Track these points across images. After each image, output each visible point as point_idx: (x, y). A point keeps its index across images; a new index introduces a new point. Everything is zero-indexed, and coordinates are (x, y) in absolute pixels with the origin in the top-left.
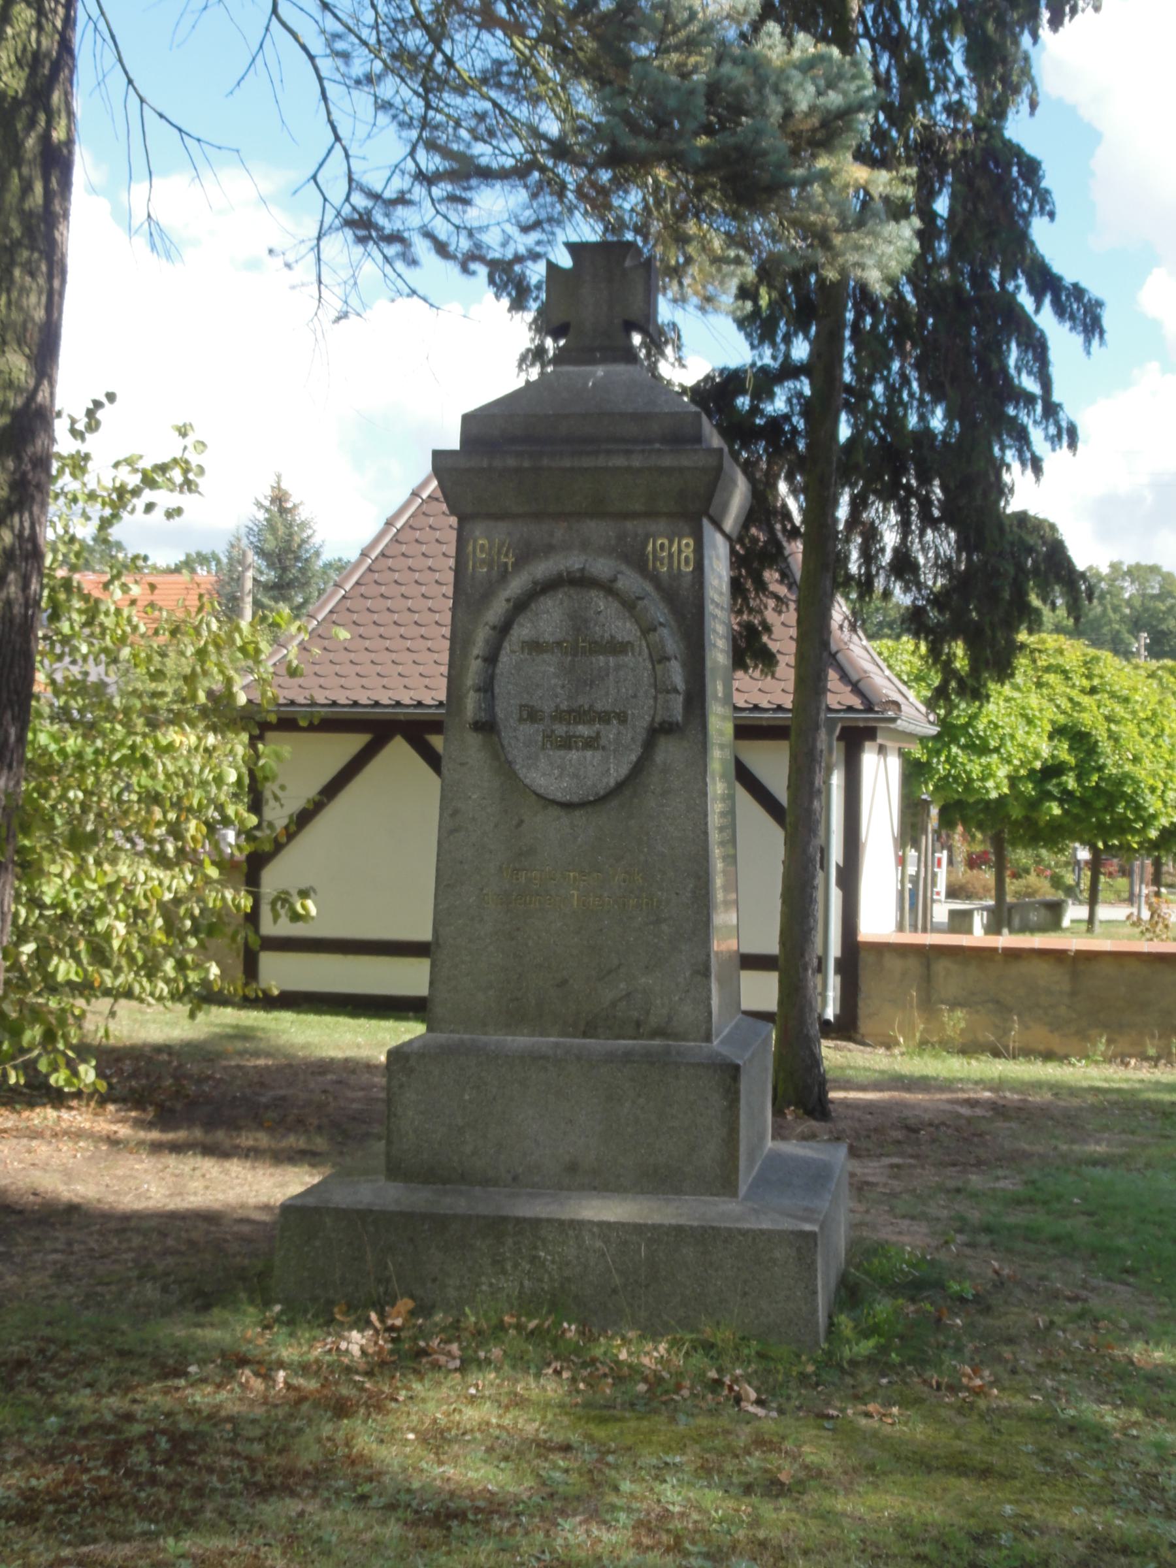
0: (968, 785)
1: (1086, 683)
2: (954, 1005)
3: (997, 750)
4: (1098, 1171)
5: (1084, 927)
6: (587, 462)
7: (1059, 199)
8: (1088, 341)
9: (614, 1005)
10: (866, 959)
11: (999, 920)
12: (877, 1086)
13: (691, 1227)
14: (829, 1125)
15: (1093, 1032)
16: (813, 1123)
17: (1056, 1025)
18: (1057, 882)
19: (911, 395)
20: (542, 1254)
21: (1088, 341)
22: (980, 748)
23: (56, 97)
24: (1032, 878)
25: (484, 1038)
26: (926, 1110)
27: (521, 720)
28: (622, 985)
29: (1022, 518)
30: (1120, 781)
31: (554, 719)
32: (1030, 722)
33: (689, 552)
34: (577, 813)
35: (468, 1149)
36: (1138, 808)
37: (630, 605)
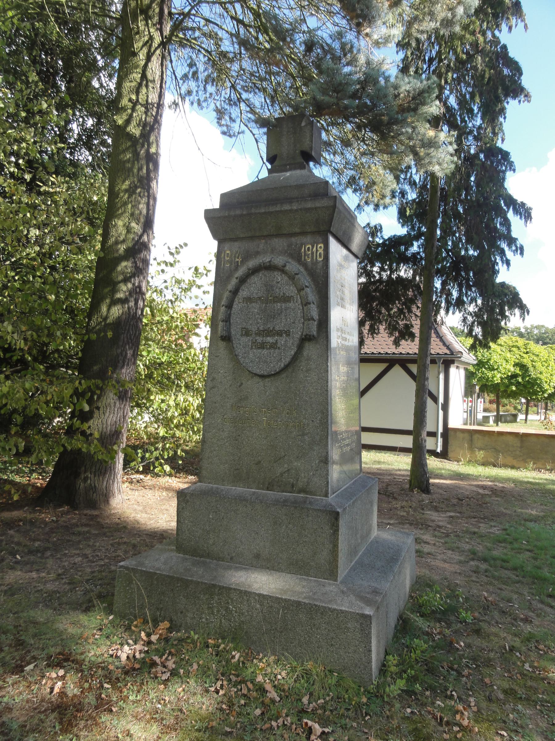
0: (487, 380)
1: (525, 351)
2: (480, 449)
3: (497, 369)
4: (531, 525)
5: (524, 421)
6: (272, 209)
7: (517, 164)
8: (526, 221)
9: (282, 475)
10: (451, 434)
11: (498, 419)
12: (451, 478)
13: (305, 603)
14: (430, 496)
15: (528, 460)
16: (424, 495)
17: (515, 457)
18: (515, 408)
19: (463, 245)
20: (231, 607)
21: (526, 221)
22: (492, 369)
23: (152, 138)
24: (508, 407)
25: (222, 487)
26: (467, 490)
27: (242, 335)
28: (286, 466)
29: (503, 284)
30: (535, 380)
31: (256, 334)
32: (507, 361)
33: (321, 251)
34: (267, 380)
35: (211, 542)
36: (541, 388)
37: (292, 277)
